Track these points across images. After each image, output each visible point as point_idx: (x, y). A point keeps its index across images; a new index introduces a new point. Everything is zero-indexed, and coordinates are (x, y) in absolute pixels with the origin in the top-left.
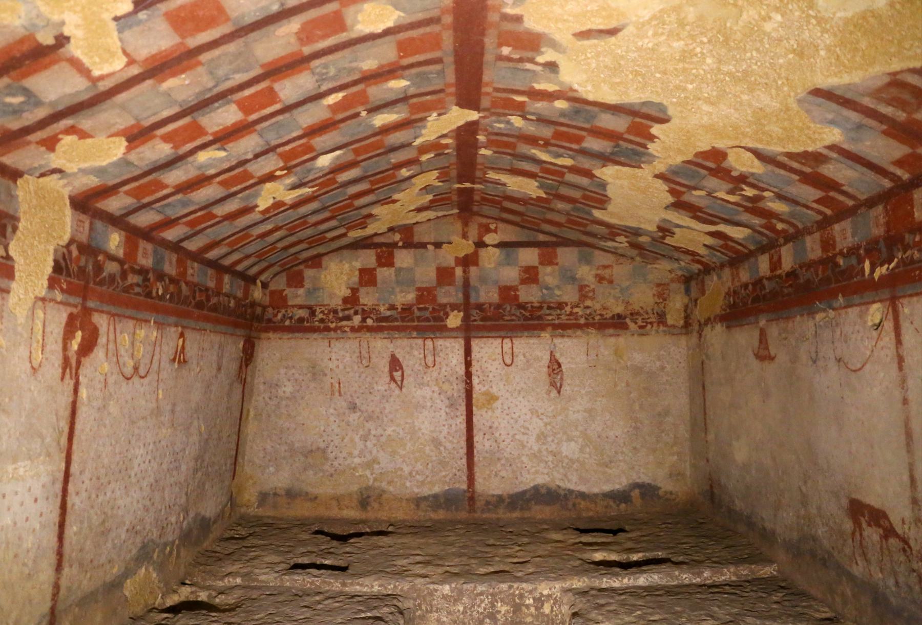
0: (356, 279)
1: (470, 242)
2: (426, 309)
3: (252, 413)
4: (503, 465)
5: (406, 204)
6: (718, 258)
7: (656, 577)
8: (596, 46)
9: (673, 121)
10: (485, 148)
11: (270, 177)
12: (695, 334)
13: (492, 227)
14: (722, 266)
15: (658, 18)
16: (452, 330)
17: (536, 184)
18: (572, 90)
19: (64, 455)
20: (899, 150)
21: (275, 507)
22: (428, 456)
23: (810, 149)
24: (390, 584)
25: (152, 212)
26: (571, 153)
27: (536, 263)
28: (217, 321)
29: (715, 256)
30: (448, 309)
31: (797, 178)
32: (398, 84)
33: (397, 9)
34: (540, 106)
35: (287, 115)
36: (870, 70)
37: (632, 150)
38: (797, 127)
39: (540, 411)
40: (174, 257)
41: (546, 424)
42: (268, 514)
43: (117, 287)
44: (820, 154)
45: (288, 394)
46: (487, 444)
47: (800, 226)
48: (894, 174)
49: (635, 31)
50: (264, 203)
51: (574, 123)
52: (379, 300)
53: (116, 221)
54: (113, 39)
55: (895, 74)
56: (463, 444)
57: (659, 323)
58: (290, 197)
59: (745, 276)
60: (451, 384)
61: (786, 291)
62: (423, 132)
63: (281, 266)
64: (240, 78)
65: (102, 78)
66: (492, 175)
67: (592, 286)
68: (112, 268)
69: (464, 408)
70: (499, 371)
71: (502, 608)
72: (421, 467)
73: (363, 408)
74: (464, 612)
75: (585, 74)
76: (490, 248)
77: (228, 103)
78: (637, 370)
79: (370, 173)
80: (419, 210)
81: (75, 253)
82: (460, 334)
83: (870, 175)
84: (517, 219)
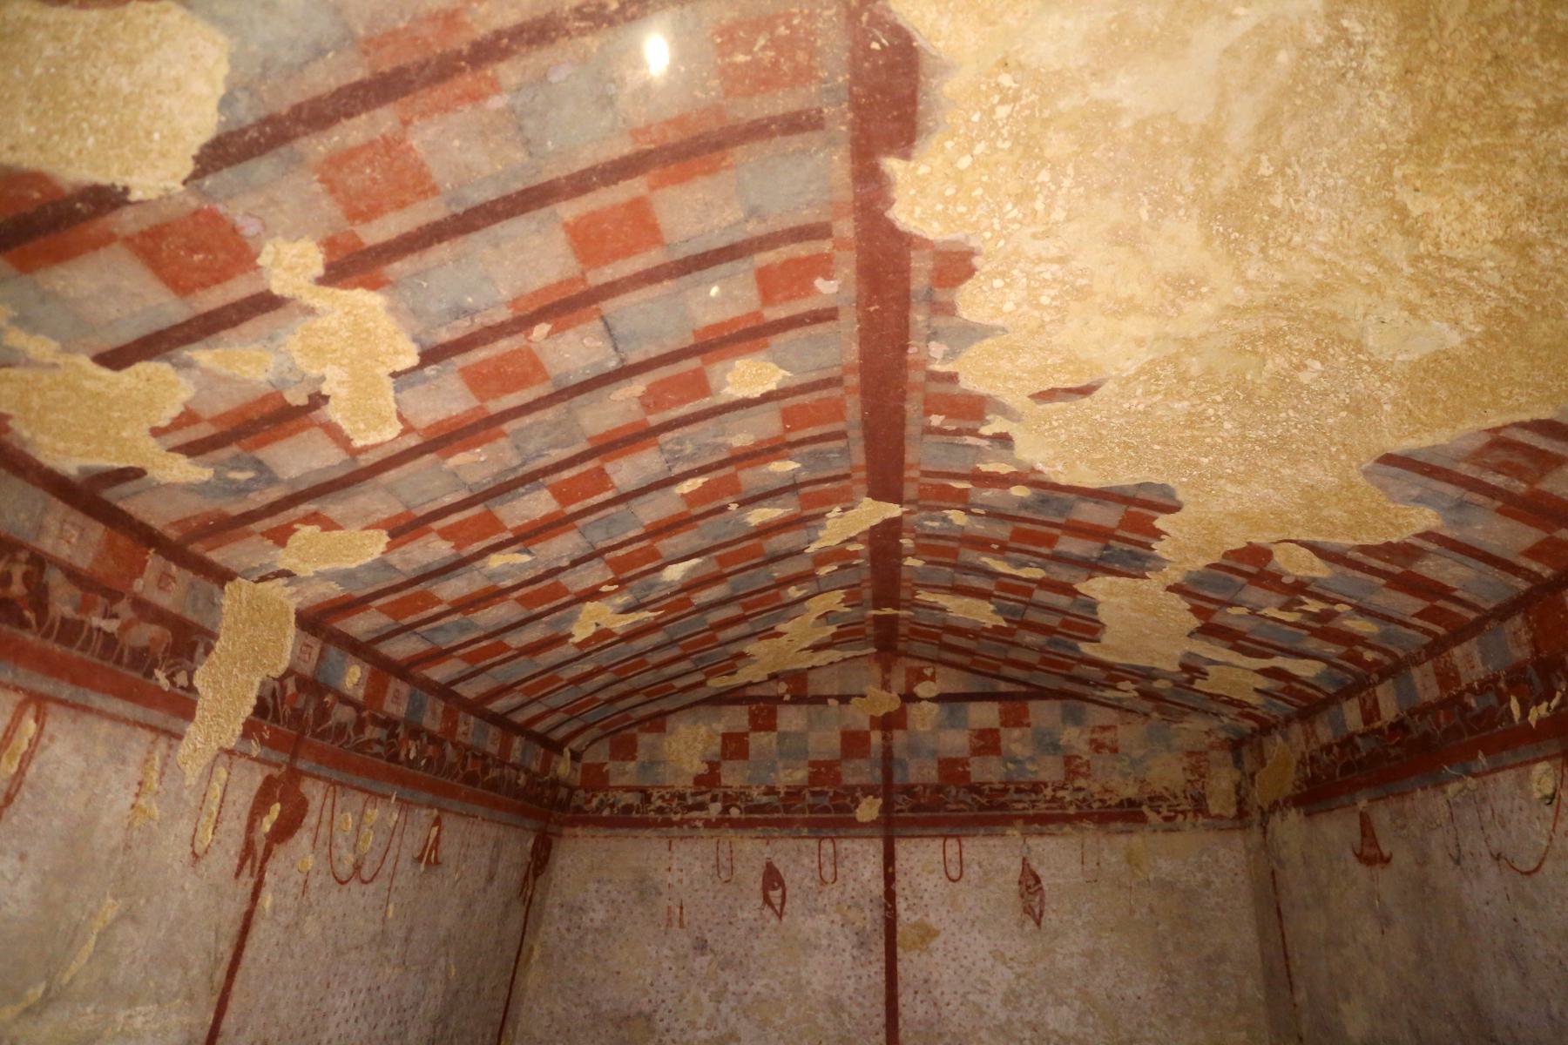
0: (716, 748)
1: (894, 694)
2: (824, 793)
3: (536, 953)
5: (797, 638)
6: (1281, 708)
8: (1064, 410)
9: (1185, 509)
10: (913, 556)
11: (593, 594)
12: (1256, 830)
13: (928, 672)
14: (1288, 721)
15: (1149, 372)
16: (864, 825)
17: (992, 607)
18: (1033, 470)
19: (215, 999)
20: (1530, 536)
23: (1395, 540)
25: (414, 638)
26: (1039, 560)
27: (996, 725)
28: (495, 805)
29: (1275, 705)
30: (858, 794)
31: (1383, 581)
32: (783, 467)
33: (781, 367)
34: (989, 494)
35: (622, 507)
36: (1460, 427)
37: (1130, 552)
38: (1369, 510)
39: (1009, 954)
40: (440, 706)
41: (1019, 976)
43: (347, 742)
44: (1412, 546)
45: (597, 924)
47: (1401, 654)
48: (1530, 571)
49: (1117, 390)
50: (581, 631)
51: (1041, 518)
53: (357, 648)
54: (387, 401)
55: (1496, 430)
58: (621, 624)
59: (1325, 734)
60: (862, 910)
61: (1393, 752)
62: (821, 533)
63: (603, 728)
65: (365, 449)
66: (924, 596)
67: (1086, 758)
68: (343, 714)
69: (883, 949)
75: (1050, 449)
76: (924, 703)
80: (816, 648)
81: (291, 688)
83: (1494, 574)
84: (965, 660)
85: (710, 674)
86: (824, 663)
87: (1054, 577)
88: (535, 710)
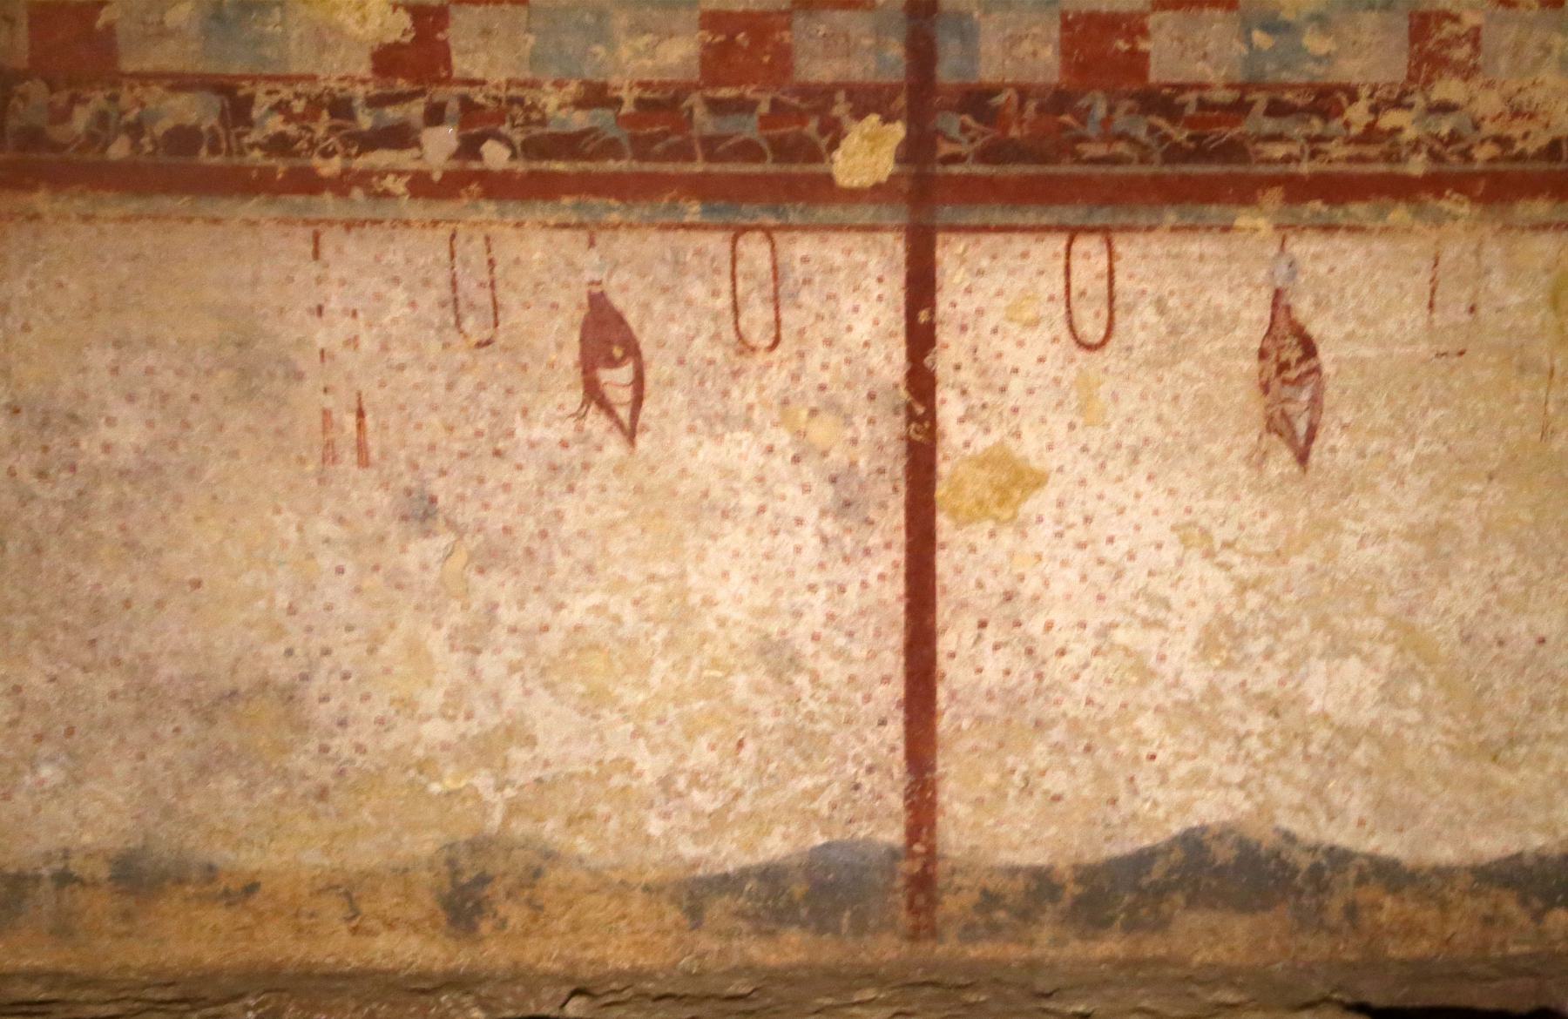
2: (743, 106)
4: (1057, 748)
16: (854, 196)
21: (63, 930)
22: (744, 711)
30: (840, 109)
39: (1220, 534)
41: (1243, 587)
45: (125, 458)
46: (993, 666)
52: (535, 59)
56: (893, 661)
60: (847, 420)
67: (1471, 19)
69: (901, 518)
70: (1050, 369)
72: (711, 758)
73: (468, 514)
82: (887, 214)
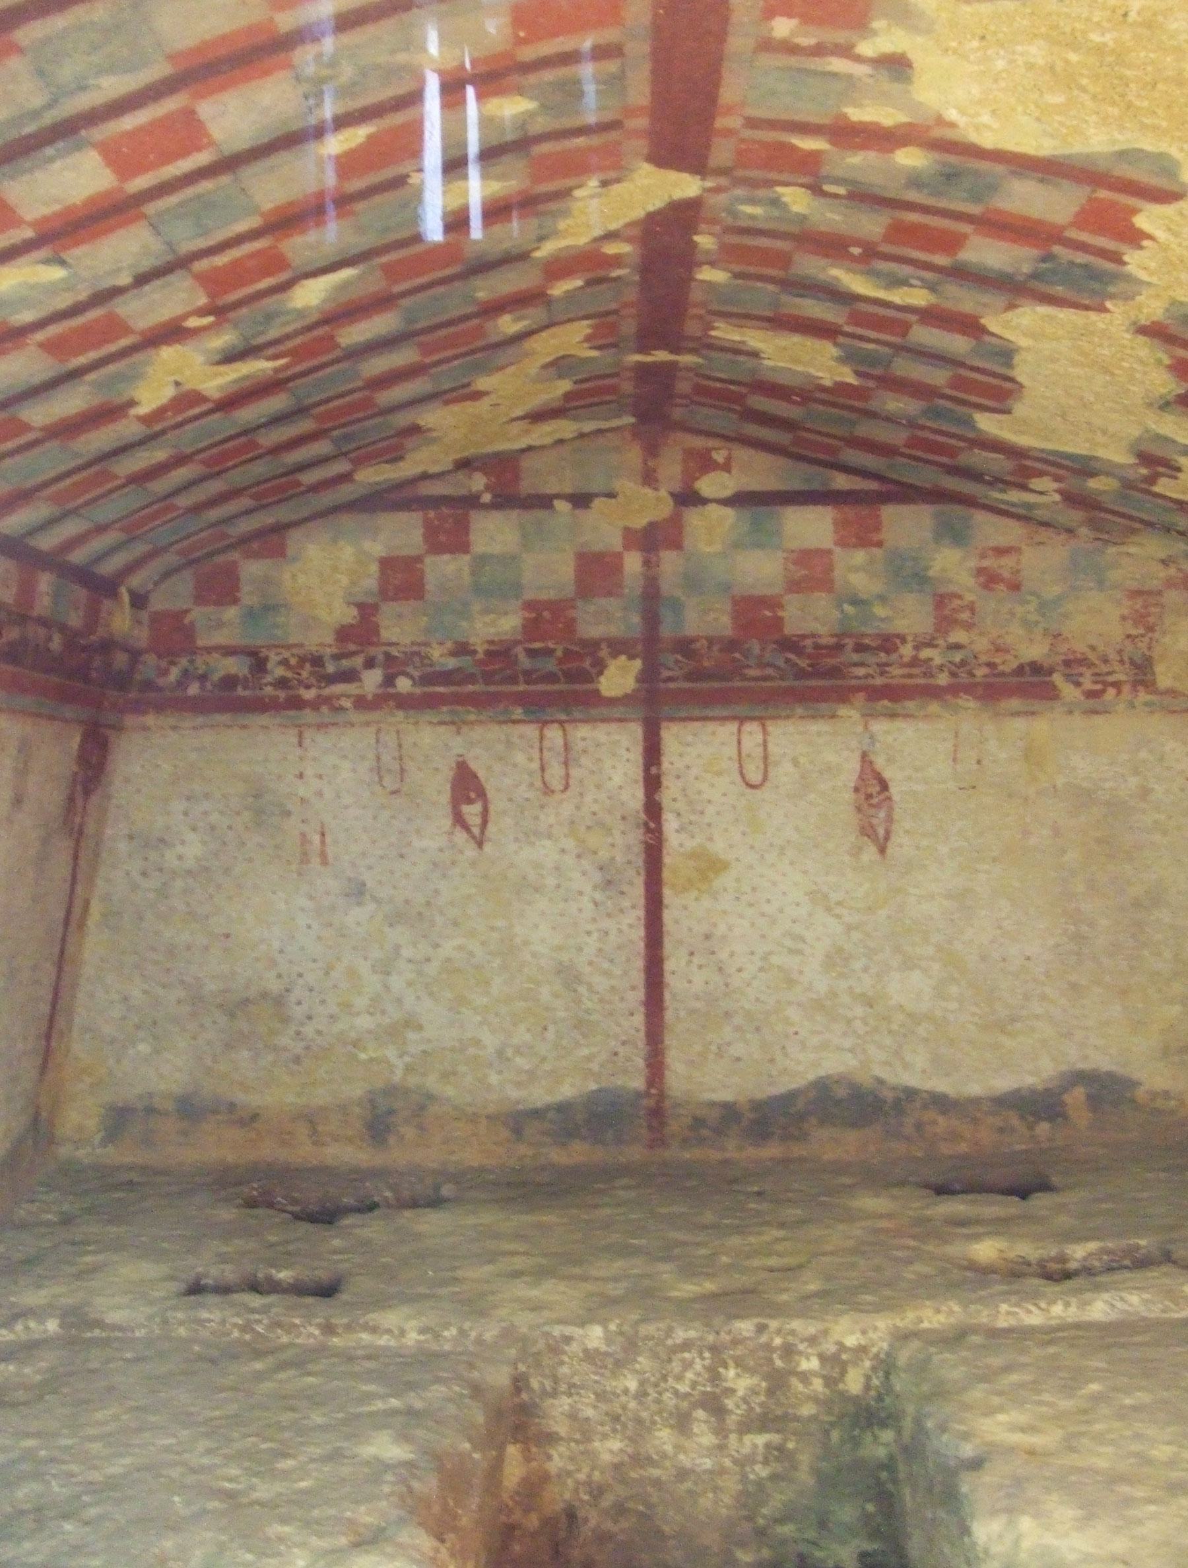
0: (370, 581)
1: (663, 493)
2: (549, 652)
4: (738, 1029)
7: (1134, 1299)
13: (719, 457)
16: (612, 702)
17: (834, 351)
18: (940, 121)
22: (547, 1009)
24: (447, 1326)
26: (928, 275)
30: (604, 652)
35: (225, 179)
37: (1085, 266)
39: (835, 897)
41: (849, 928)
42: (128, 1159)
45: (190, 863)
46: (699, 978)
50: (151, 393)
56: (637, 976)
57: (1136, 684)
58: (217, 382)
60: (608, 831)
62: (562, 225)
64: (112, 86)
66: (724, 332)
67: (969, 597)
71: (739, 1382)
72: (528, 1037)
74: (641, 1395)
76: (712, 507)
77: (78, 148)
78: (1083, 797)
79: (418, 326)
80: (538, 417)
85: (359, 462)
86: (548, 441)
87: (948, 305)
88: (71, 528)
